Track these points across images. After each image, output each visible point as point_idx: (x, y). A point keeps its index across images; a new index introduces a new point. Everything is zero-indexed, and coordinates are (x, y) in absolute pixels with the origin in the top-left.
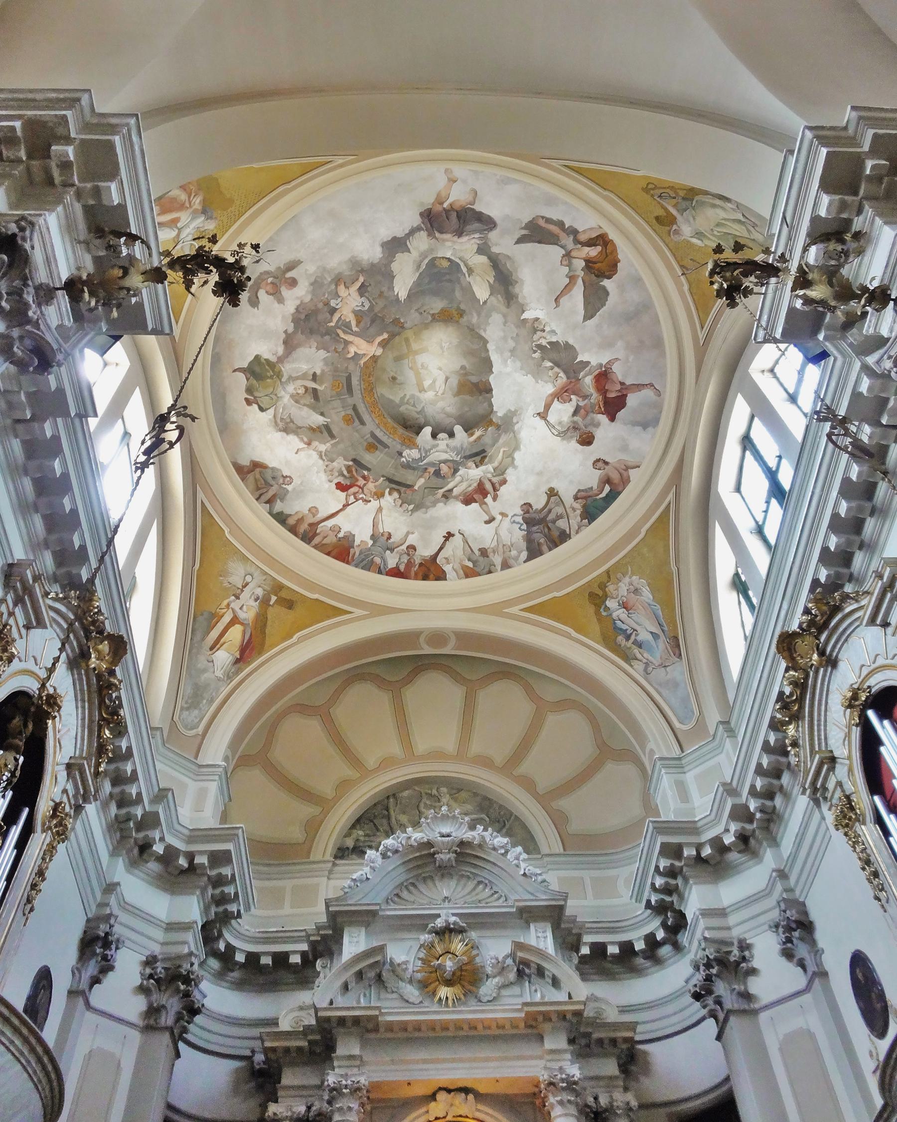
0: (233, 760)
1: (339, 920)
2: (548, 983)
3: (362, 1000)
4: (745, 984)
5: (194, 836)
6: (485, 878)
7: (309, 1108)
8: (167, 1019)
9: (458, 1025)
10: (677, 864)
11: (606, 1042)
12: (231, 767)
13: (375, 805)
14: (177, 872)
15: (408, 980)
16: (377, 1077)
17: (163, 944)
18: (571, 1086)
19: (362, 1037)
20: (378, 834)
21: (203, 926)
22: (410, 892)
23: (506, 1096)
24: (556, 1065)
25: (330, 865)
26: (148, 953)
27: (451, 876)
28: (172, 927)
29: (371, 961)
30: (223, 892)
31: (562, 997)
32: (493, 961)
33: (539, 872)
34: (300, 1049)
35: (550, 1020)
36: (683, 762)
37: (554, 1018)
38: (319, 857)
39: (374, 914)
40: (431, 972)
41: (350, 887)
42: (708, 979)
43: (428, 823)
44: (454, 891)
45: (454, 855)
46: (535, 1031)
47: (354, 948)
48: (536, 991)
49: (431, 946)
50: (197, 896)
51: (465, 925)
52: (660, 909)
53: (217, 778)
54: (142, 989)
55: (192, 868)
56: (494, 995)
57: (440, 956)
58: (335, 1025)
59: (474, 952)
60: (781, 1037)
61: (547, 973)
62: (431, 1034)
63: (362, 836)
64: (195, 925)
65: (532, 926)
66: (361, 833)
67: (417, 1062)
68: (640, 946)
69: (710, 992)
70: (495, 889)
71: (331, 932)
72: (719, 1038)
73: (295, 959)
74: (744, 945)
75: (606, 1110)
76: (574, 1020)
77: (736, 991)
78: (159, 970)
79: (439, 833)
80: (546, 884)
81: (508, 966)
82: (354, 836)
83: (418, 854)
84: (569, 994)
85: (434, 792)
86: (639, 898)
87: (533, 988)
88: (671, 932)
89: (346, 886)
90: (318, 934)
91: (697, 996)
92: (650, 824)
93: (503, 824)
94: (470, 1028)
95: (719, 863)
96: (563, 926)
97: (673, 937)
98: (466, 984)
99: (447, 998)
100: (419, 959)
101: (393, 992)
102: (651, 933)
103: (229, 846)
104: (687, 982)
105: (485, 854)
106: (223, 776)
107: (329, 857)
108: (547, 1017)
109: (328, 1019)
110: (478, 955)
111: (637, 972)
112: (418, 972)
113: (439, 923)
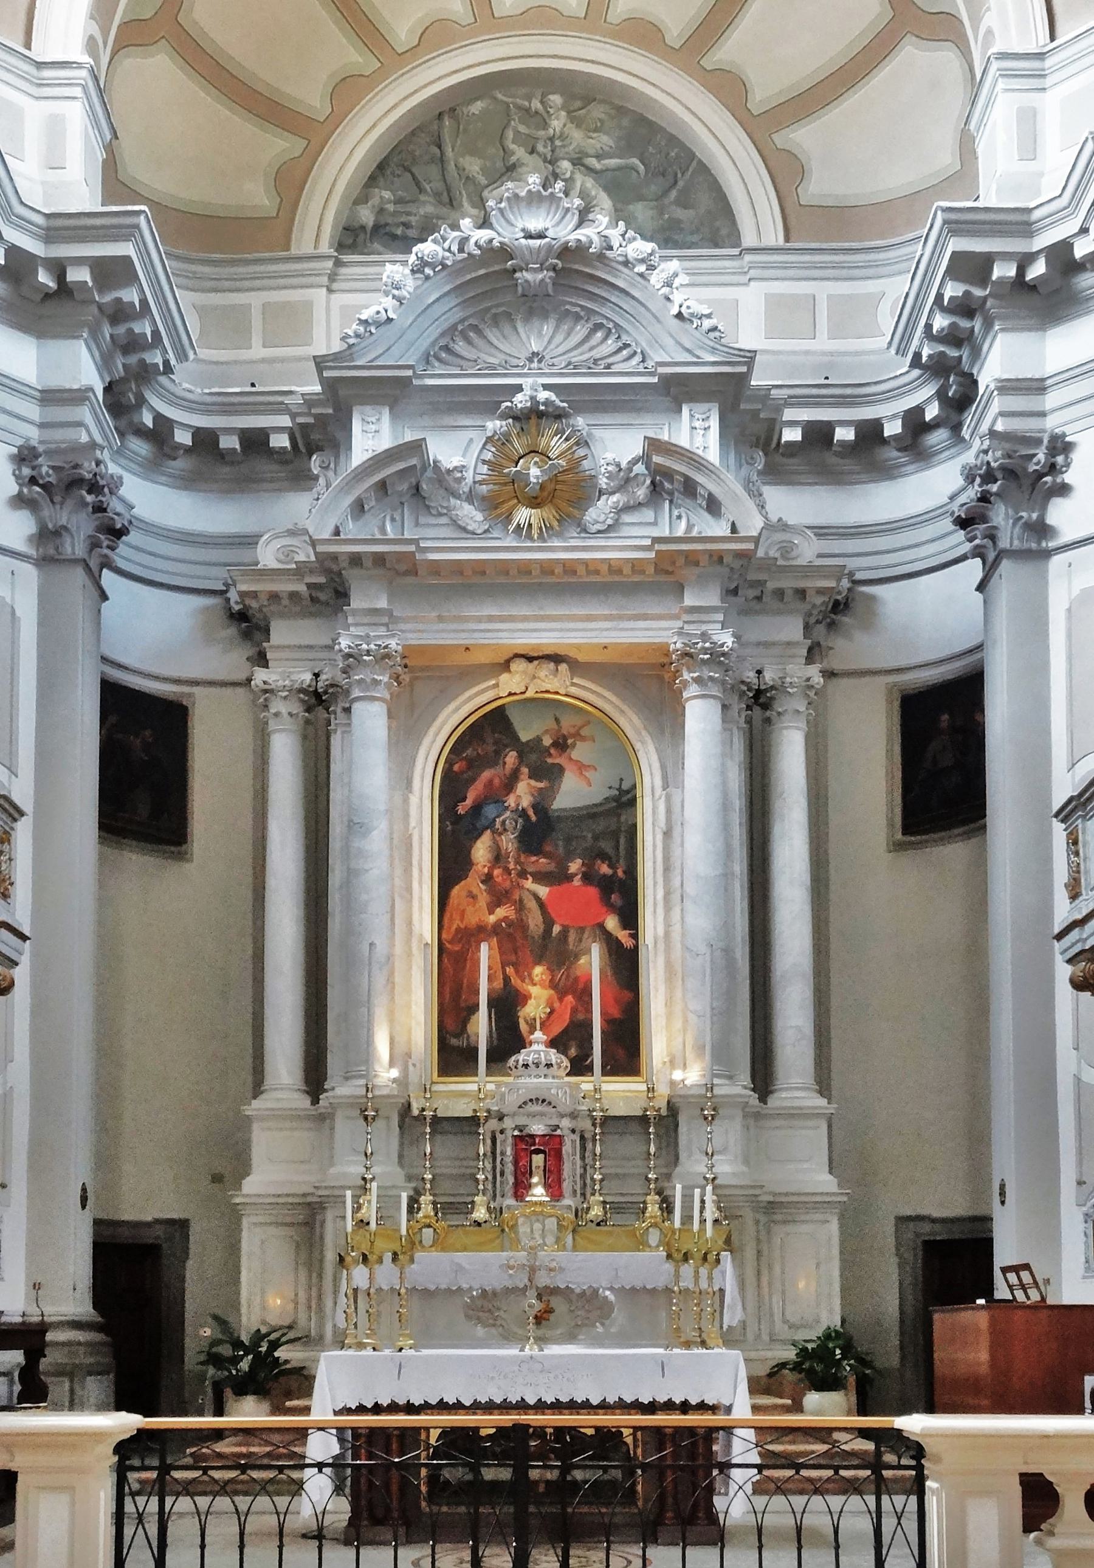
0: (105, 44)
1: (342, 392)
2: (700, 505)
3: (388, 528)
4: (1043, 508)
5: (56, 229)
6: (607, 318)
7: (317, 675)
8: (75, 546)
9: (547, 568)
10: (978, 292)
11: (789, 593)
12: (105, 60)
13: (413, 133)
14: (38, 297)
15: (464, 497)
16: (414, 639)
17: (42, 426)
18: (717, 657)
19: (391, 583)
20: (422, 198)
21: (108, 389)
22: (469, 342)
23: (620, 667)
24: (694, 629)
25: (330, 264)
26: (20, 442)
27: (545, 315)
28: (50, 397)
29: (401, 466)
30: (130, 331)
31: (719, 529)
32: (610, 468)
33: (706, 312)
34: (294, 596)
35: (697, 564)
36: (1049, 62)
37: (704, 560)
38: (308, 249)
39: (405, 382)
40: (505, 484)
41: (357, 336)
42: (984, 498)
43: (501, 211)
44: (549, 342)
45: (552, 274)
46: (671, 579)
47: (370, 442)
48: (679, 517)
49: (507, 438)
50: (85, 340)
51: (565, 405)
52: (938, 368)
53: (78, 92)
54: (20, 501)
55: (64, 290)
56: (610, 522)
57: (520, 458)
58: (345, 564)
59: (581, 452)
60: (1076, 592)
61: (700, 490)
62: (502, 580)
63: (389, 202)
64: (91, 394)
65: (685, 409)
66: (387, 194)
67: (479, 619)
68: (893, 428)
69: (984, 519)
70: (625, 338)
71: (330, 411)
72: (981, 587)
73: (281, 441)
74: (1059, 445)
75: (772, 688)
76: (737, 564)
77: (1023, 521)
78: (44, 469)
79: (523, 230)
80: (717, 334)
81: (637, 475)
82: (375, 201)
83: (482, 272)
84: (733, 524)
85: (536, 105)
86: (902, 347)
87: (676, 513)
88: (952, 407)
89: (351, 333)
90: (309, 414)
91: (963, 523)
92: (939, 213)
93: (672, 181)
94: (565, 572)
95: (1057, 291)
96: (742, 406)
97: (954, 417)
98: (563, 505)
99: (530, 525)
100: (484, 462)
101: (440, 515)
102: (917, 406)
103: (126, 249)
104: (952, 498)
105: (609, 273)
106: (91, 84)
107: (325, 248)
108: (691, 559)
109: (334, 557)
110: (585, 457)
111: (886, 472)
112: (481, 483)
113: (521, 401)
